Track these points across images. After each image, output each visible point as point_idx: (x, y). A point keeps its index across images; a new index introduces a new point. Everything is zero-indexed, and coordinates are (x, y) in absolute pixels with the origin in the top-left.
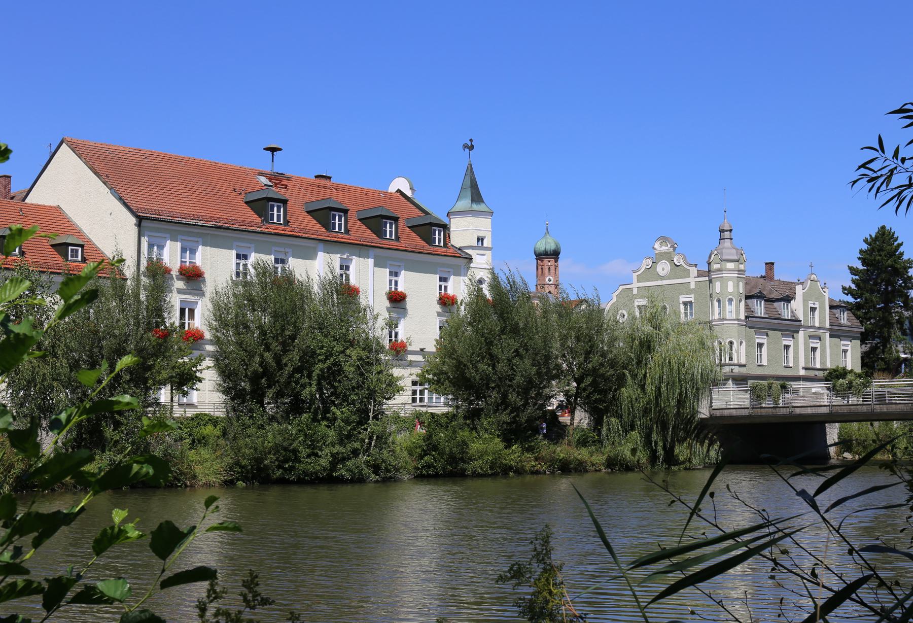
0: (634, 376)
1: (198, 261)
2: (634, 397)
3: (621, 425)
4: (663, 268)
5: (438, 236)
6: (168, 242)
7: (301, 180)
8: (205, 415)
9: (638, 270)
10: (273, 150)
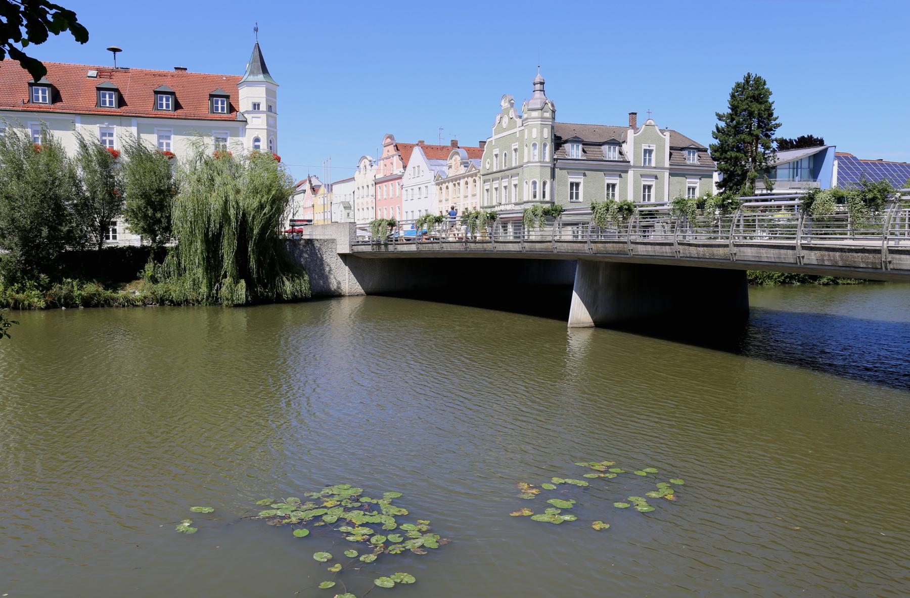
10: (115, 50)
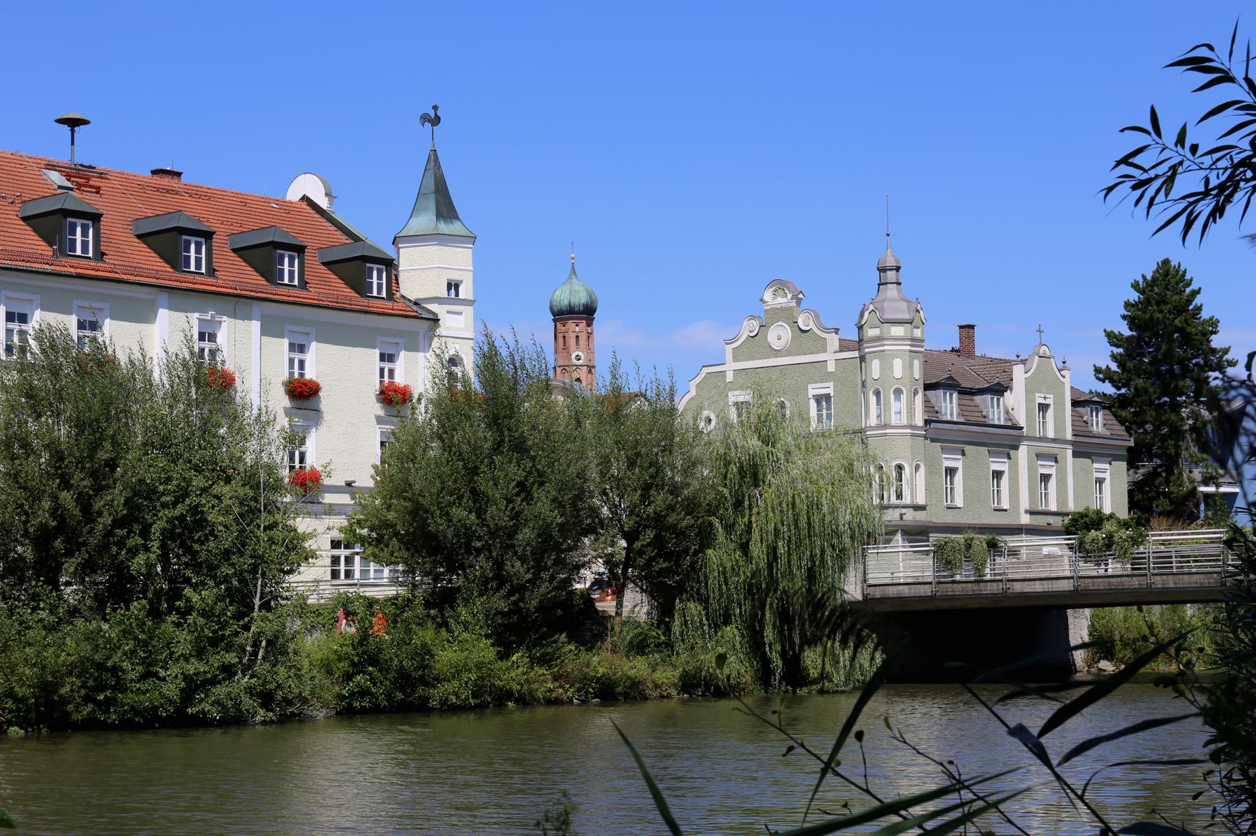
0: (729, 528)
2: (729, 565)
3: (707, 614)
4: (779, 335)
5: (377, 280)
7: (124, 178)
10: (73, 123)
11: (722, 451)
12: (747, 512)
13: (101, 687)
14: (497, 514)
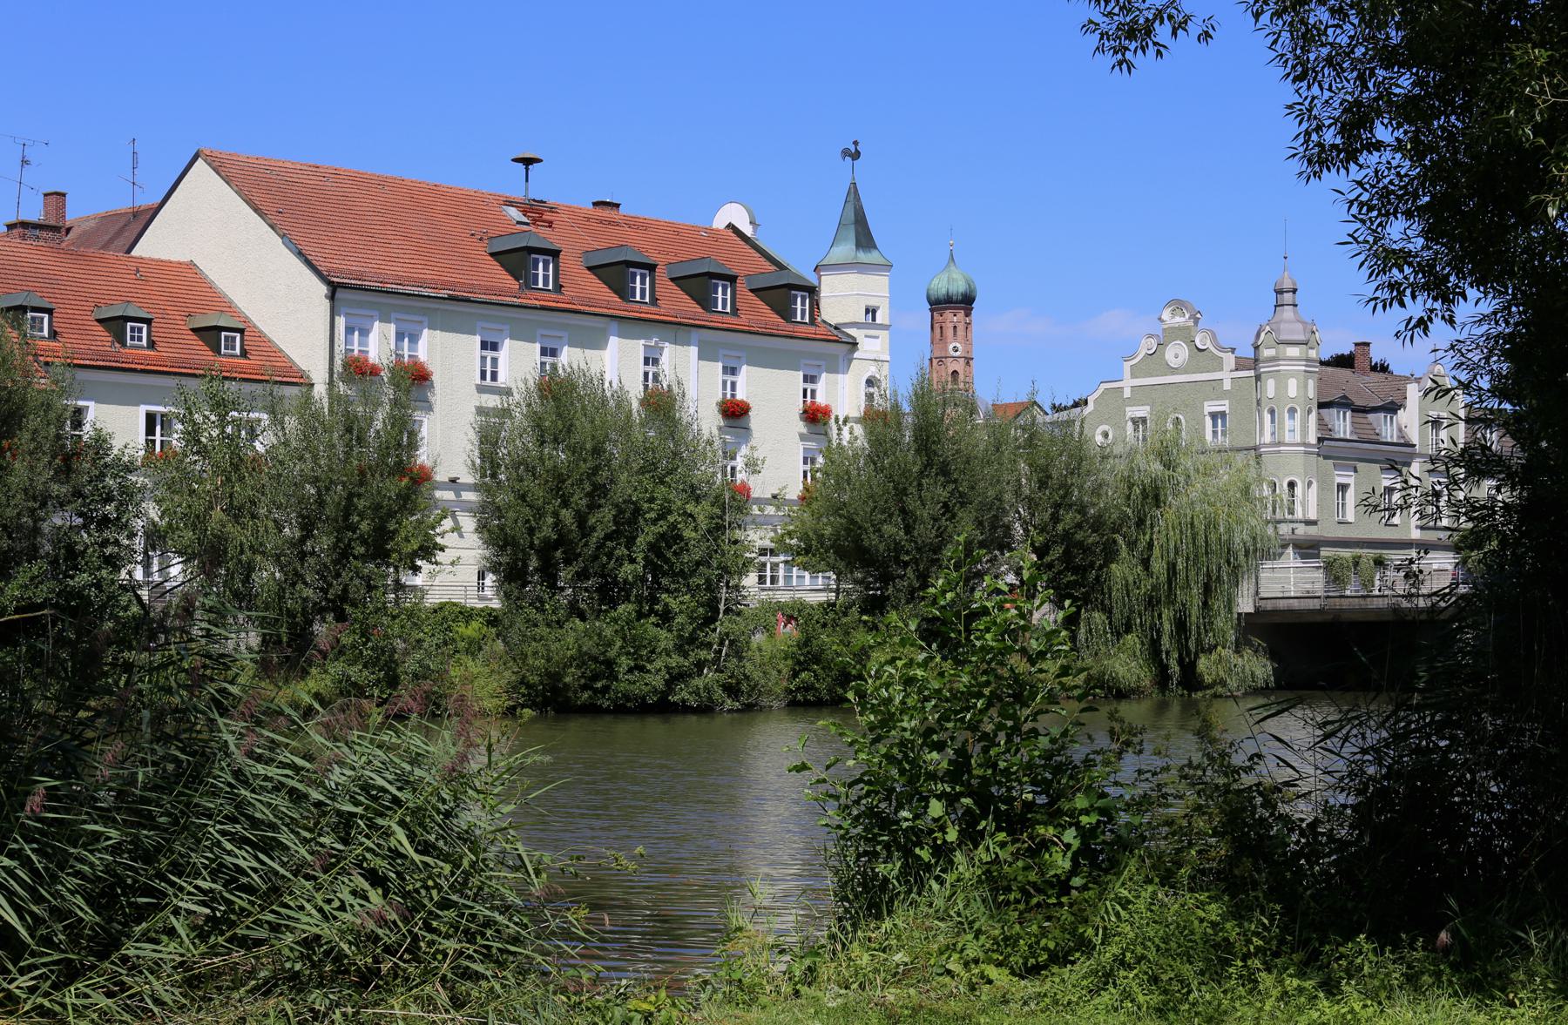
0: (1132, 545)
1: (422, 353)
2: (1131, 579)
3: (1110, 623)
4: (1176, 354)
5: (800, 306)
6: (377, 324)
7: (572, 211)
8: (455, 604)
9: (1132, 357)
10: (528, 162)
11: (1126, 474)
12: (1149, 531)
13: (595, 678)
14: (925, 532)
